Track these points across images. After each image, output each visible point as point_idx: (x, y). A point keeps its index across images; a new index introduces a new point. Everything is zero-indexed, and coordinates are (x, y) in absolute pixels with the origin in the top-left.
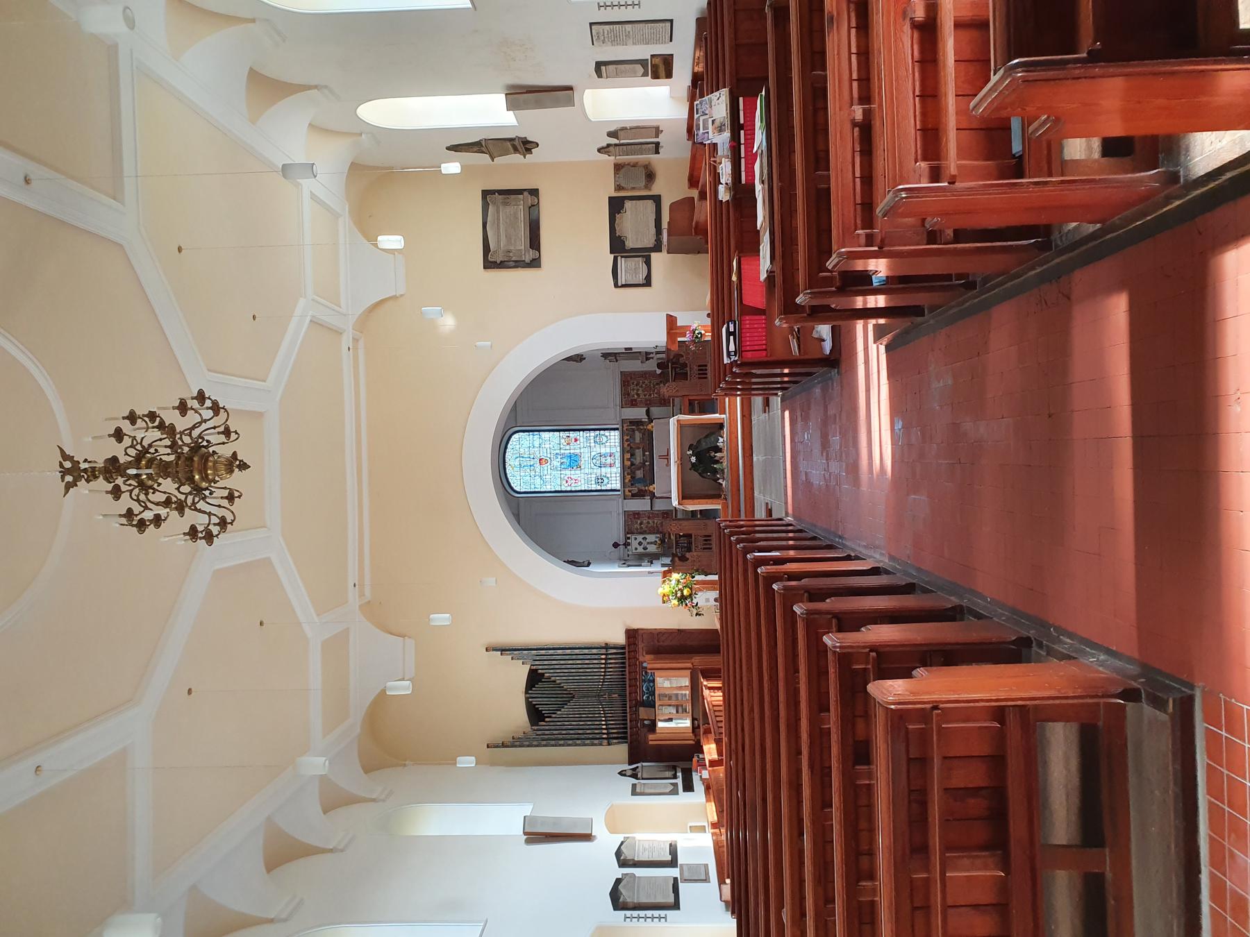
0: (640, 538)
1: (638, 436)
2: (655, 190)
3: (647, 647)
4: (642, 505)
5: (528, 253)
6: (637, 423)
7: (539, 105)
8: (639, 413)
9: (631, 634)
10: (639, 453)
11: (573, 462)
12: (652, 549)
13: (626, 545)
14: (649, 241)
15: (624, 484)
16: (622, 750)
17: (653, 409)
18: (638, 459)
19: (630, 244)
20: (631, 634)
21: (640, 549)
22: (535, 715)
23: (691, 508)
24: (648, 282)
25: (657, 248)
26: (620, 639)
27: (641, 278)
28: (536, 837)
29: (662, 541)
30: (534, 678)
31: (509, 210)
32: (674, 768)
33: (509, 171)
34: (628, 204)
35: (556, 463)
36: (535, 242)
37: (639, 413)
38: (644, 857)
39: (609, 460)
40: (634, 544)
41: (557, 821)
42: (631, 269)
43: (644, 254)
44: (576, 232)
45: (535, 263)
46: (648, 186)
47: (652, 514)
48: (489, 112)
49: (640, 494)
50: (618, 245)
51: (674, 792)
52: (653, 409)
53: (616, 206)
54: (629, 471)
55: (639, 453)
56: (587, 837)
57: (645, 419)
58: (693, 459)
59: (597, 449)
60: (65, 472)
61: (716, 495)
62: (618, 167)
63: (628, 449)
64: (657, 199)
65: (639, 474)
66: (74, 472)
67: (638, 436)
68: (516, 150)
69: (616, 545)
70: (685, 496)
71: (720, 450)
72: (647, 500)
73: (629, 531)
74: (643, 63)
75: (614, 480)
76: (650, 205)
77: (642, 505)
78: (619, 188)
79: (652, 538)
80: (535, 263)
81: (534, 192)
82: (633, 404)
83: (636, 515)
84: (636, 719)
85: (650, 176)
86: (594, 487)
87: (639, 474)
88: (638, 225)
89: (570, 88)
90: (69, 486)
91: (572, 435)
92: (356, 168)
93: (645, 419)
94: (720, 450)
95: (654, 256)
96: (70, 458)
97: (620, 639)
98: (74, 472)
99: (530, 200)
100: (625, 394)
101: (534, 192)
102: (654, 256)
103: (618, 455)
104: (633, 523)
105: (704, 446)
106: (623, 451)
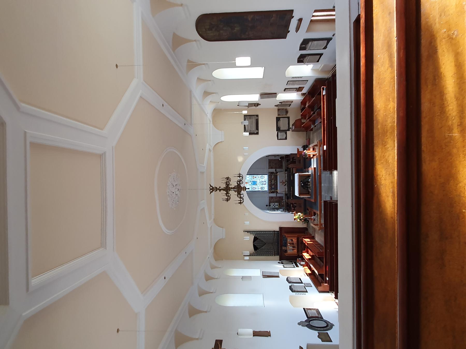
0: (273, 204)
1: (273, 176)
2: (288, 116)
3: (284, 232)
4: (274, 195)
5: (254, 131)
6: (272, 173)
7: (268, 97)
8: (273, 170)
9: (281, 228)
10: (273, 181)
11: (254, 183)
12: (277, 207)
13: (270, 206)
14: (287, 128)
15: (269, 190)
16: (278, 257)
17: (277, 170)
18: (273, 183)
19: (281, 129)
20: (281, 228)
21: (273, 207)
22: (255, 248)
23: (302, 197)
24: (286, 139)
25: (289, 130)
26: (277, 229)
27: (284, 138)
28: (265, 276)
29: (279, 205)
30: (255, 239)
31: (251, 120)
32: (292, 262)
33: (254, 111)
34: (281, 119)
35: (250, 183)
36: (257, 129)
37: (273, 170)
38: (294, 281)
39: (264, 183)
40: (272, 205)
41: (271, 272)
42: (281, 135)
43: (285, 131)
44: (268, 126)
45: (257, 133)
46: (286, 115)
47: (276, 197)
48: (255, 98)
49: (273, 192)
50: (278, 129)
51: (294, 267)
52: (277, 170)
53: (278, 119)
54: (270, 186)
55: (273, 181)
56: (278, 277)
57: (275, 172)
58: (302, 184)
59: (261, 180)
60: (211, 189)
61: (308, 193)
62: (279, 110)
63: (270, 180)
64: (289, 118)
65: (273, 187)
66: (213, 189)
67: (273, 176)
68: (255, 106)
69: (267, 206)
70: (300, 194)
71: (309, 182)
72: (275, 194)
73: (270, 202)
74: (296, 88)
75: (266, 188)
76: (287, 119)
77: (274, 195)
78: (279, 115)
79: (276, 204)
80: (257, 133)
81: (257, 116)
82: (272, 168)
83: (272, 197)
84: (281, 249)
85: (287, 112)
86: (260, 190)
87: (273, 187)
88: (283, 124)
89: (276, 94)
90: (211, 192)
91: (255, 176)
92: (215, 110)
93: (275, 172)
94: (309, 182)
95: (288, 132)
96: (212, 186)
97: (277, 229)
98: (213, 189)
99: (256, 118)
100: (269, 165)
101: (257, 116)
102: (288, 132)
103: (267, 182)
104: (271, 200)
105: (305, 181)
106: (269, 180)
